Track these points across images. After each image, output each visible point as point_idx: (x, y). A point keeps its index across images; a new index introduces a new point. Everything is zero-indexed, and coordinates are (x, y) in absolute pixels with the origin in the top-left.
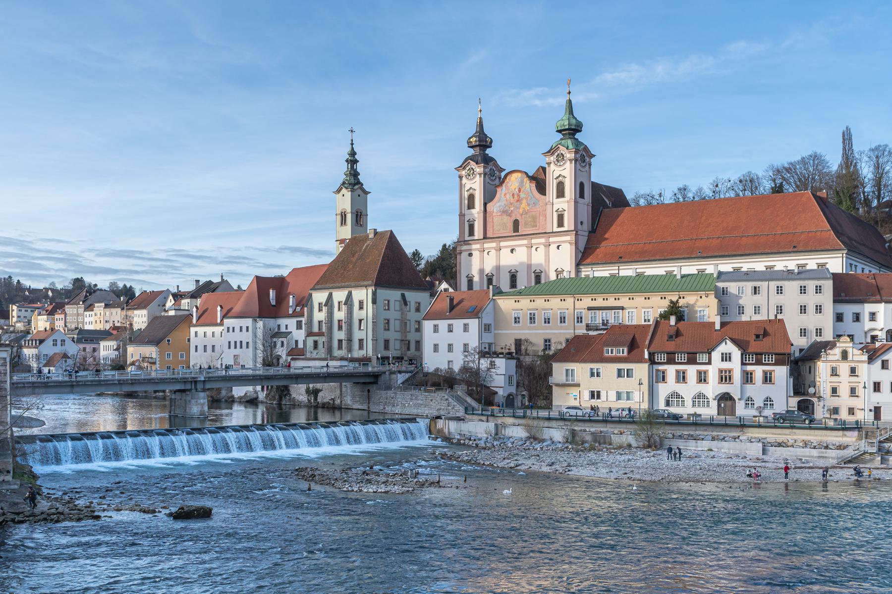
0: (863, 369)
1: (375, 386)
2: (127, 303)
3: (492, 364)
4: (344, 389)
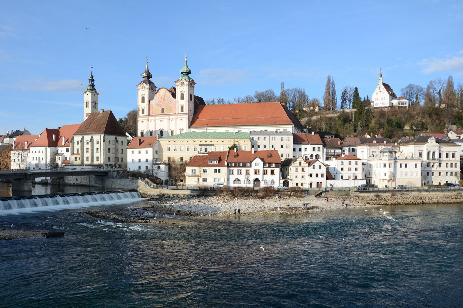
0: (307, 169)
1: (106, 177)
3: (159, 168)
4: (91, 178)
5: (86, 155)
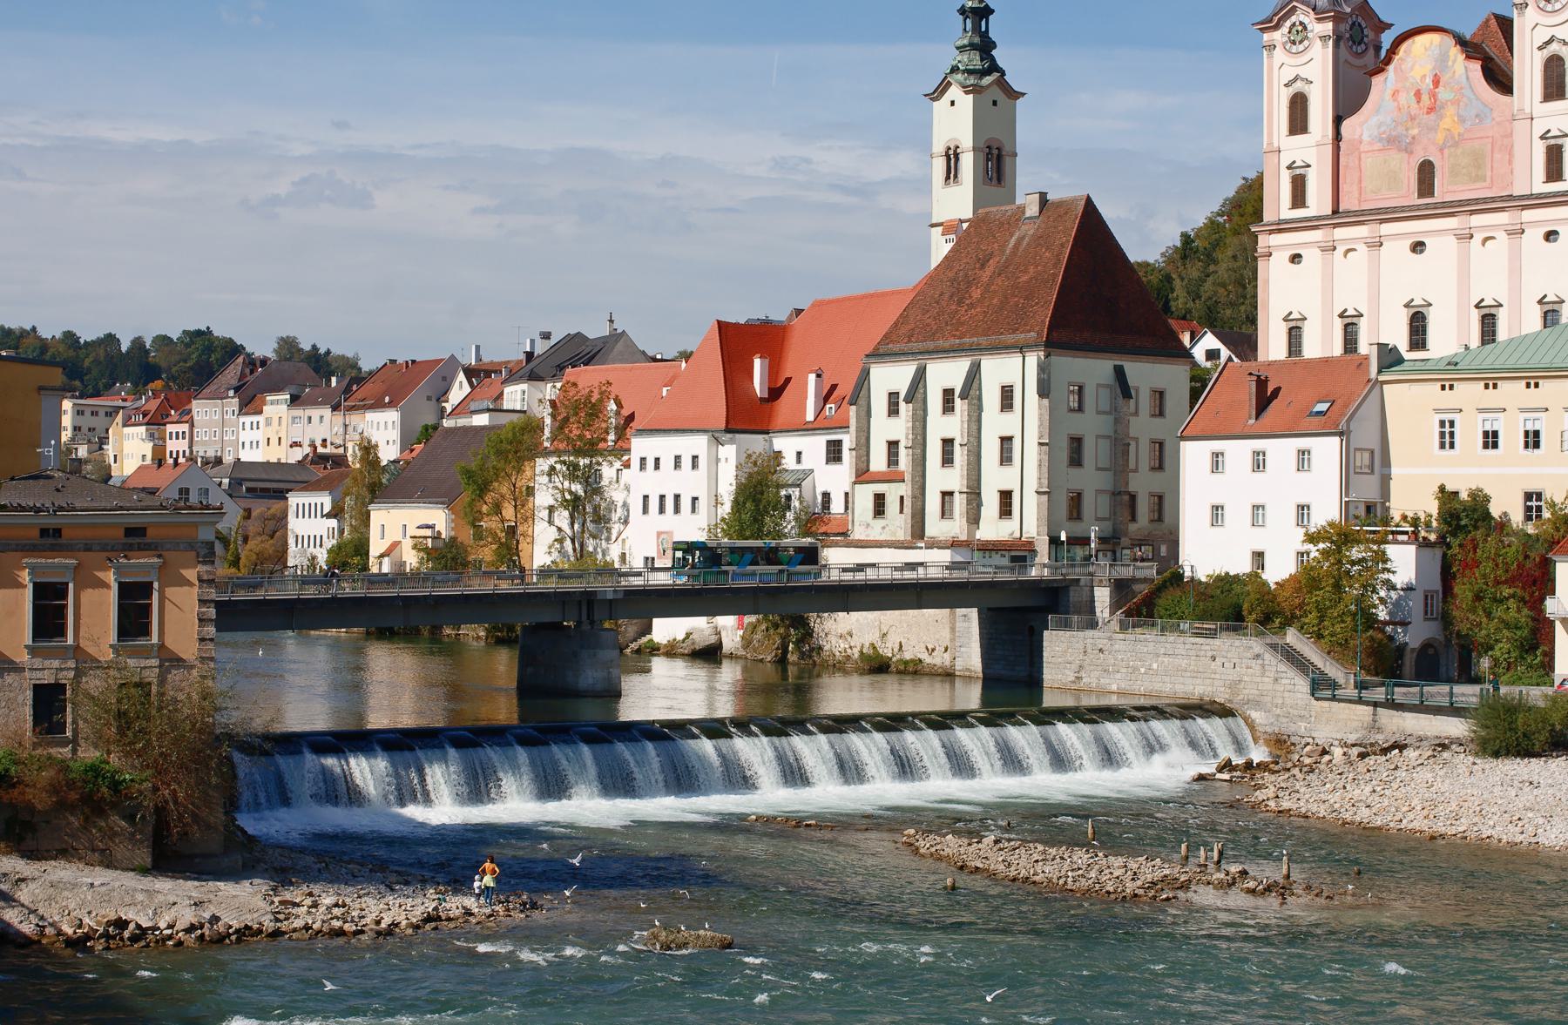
2: (347, 391)
4: (959, 625)
5: (940, 479)
